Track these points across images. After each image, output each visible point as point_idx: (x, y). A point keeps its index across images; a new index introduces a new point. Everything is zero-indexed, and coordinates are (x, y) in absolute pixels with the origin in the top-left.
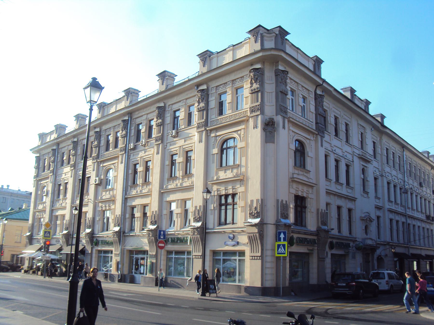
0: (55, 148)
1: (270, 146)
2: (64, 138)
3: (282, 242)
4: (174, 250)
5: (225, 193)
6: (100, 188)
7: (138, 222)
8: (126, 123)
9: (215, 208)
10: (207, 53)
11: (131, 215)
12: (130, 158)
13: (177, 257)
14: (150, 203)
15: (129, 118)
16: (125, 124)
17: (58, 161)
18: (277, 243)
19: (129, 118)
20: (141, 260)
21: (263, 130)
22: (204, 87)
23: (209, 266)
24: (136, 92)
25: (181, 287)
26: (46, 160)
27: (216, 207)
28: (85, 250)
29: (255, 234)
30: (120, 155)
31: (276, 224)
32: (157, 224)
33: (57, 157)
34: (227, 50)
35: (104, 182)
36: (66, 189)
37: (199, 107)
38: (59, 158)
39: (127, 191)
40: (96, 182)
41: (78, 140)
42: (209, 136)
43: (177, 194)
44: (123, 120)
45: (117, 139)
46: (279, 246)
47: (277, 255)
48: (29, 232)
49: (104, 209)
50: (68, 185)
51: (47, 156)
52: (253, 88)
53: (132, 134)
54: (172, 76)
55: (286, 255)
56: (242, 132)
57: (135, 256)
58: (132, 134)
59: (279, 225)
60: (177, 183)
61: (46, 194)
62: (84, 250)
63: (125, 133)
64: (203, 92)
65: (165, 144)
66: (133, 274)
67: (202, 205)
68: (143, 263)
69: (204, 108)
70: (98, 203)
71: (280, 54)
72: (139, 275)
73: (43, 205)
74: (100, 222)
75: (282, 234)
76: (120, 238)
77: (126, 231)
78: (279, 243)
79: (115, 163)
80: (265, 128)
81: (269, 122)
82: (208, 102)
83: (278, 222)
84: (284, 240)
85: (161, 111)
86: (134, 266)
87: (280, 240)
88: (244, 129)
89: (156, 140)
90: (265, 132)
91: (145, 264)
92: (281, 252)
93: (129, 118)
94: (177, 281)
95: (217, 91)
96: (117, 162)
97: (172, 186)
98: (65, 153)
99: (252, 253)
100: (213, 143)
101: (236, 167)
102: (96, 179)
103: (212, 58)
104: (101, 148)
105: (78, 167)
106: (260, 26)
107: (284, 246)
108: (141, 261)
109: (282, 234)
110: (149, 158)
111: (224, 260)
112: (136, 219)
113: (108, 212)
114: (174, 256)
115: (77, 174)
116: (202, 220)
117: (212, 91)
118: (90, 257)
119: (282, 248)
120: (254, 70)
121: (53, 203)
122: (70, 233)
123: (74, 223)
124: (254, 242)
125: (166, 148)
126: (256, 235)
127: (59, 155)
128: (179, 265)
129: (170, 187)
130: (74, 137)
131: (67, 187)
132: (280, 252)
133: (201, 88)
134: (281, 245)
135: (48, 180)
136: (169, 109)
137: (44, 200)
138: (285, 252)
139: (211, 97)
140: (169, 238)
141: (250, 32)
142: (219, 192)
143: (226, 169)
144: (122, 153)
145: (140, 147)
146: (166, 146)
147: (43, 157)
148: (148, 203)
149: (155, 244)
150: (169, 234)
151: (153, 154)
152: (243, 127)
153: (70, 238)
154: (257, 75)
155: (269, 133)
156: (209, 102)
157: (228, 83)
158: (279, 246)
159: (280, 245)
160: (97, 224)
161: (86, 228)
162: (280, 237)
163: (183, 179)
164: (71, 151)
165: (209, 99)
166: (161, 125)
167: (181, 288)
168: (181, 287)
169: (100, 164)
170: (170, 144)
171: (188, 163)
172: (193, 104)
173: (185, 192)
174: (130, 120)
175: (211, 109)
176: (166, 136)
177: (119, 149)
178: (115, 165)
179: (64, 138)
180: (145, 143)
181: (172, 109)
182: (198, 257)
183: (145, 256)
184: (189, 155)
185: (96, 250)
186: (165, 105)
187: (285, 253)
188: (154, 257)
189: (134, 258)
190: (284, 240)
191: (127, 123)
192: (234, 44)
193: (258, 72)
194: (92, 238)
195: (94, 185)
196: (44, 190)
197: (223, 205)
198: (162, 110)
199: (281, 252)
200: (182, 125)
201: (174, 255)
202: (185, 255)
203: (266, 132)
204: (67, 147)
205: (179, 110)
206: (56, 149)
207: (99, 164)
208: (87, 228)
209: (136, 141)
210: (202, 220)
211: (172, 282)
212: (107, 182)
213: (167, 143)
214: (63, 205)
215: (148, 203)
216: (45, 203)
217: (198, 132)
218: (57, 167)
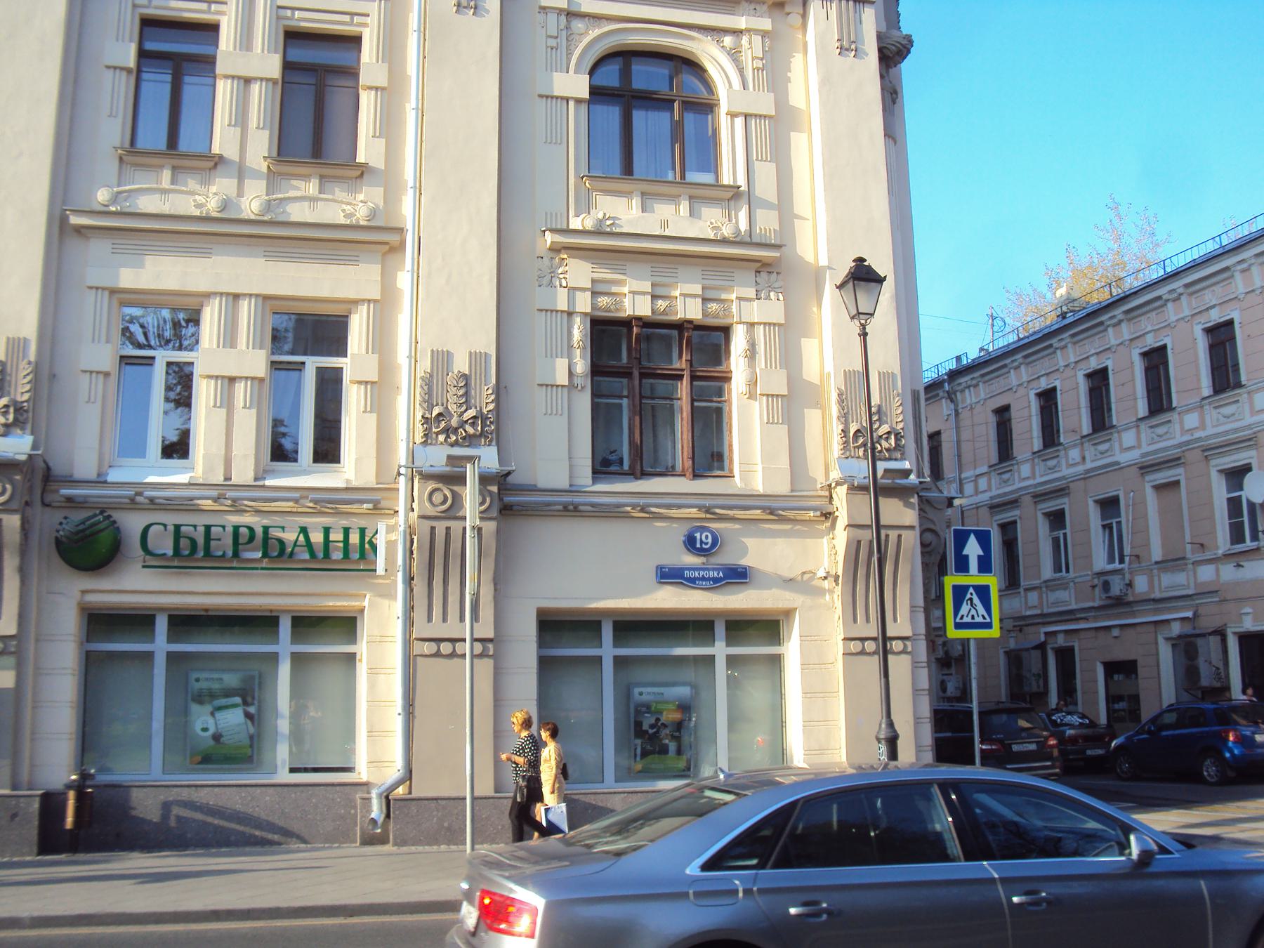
3: (974, 578)
4: (162, 609)
5: (594, 307)
25: (276, 837)
43: (216, 259)
46: (960, 592)
47: (952, 633)
67: (897, 370)
75: (972, 538)
78: (961, 580)
88: (764, 34)
92: (973, 617)
94: (235, 801)
99: (855, 621)
101: (722, 200)
107: (983, 592)
109: (972, 538)
119: (976, 600)
126: (448, 529)
128: (201, 702)
132: (967, 620)
134: (971, 590)
142: (603, 301)
143: (649, 194)
158: (960, 592)
159: (966, 588)
162: (965, 552)
163: (273, 178)
167: (279, 844)
168: (276, 837)
173: (291, 257)
187: (988, 626)
188: (874, 653)
190: (985, 566)
199: (973, 617)
202: (152, 639)
211: (176, 811)
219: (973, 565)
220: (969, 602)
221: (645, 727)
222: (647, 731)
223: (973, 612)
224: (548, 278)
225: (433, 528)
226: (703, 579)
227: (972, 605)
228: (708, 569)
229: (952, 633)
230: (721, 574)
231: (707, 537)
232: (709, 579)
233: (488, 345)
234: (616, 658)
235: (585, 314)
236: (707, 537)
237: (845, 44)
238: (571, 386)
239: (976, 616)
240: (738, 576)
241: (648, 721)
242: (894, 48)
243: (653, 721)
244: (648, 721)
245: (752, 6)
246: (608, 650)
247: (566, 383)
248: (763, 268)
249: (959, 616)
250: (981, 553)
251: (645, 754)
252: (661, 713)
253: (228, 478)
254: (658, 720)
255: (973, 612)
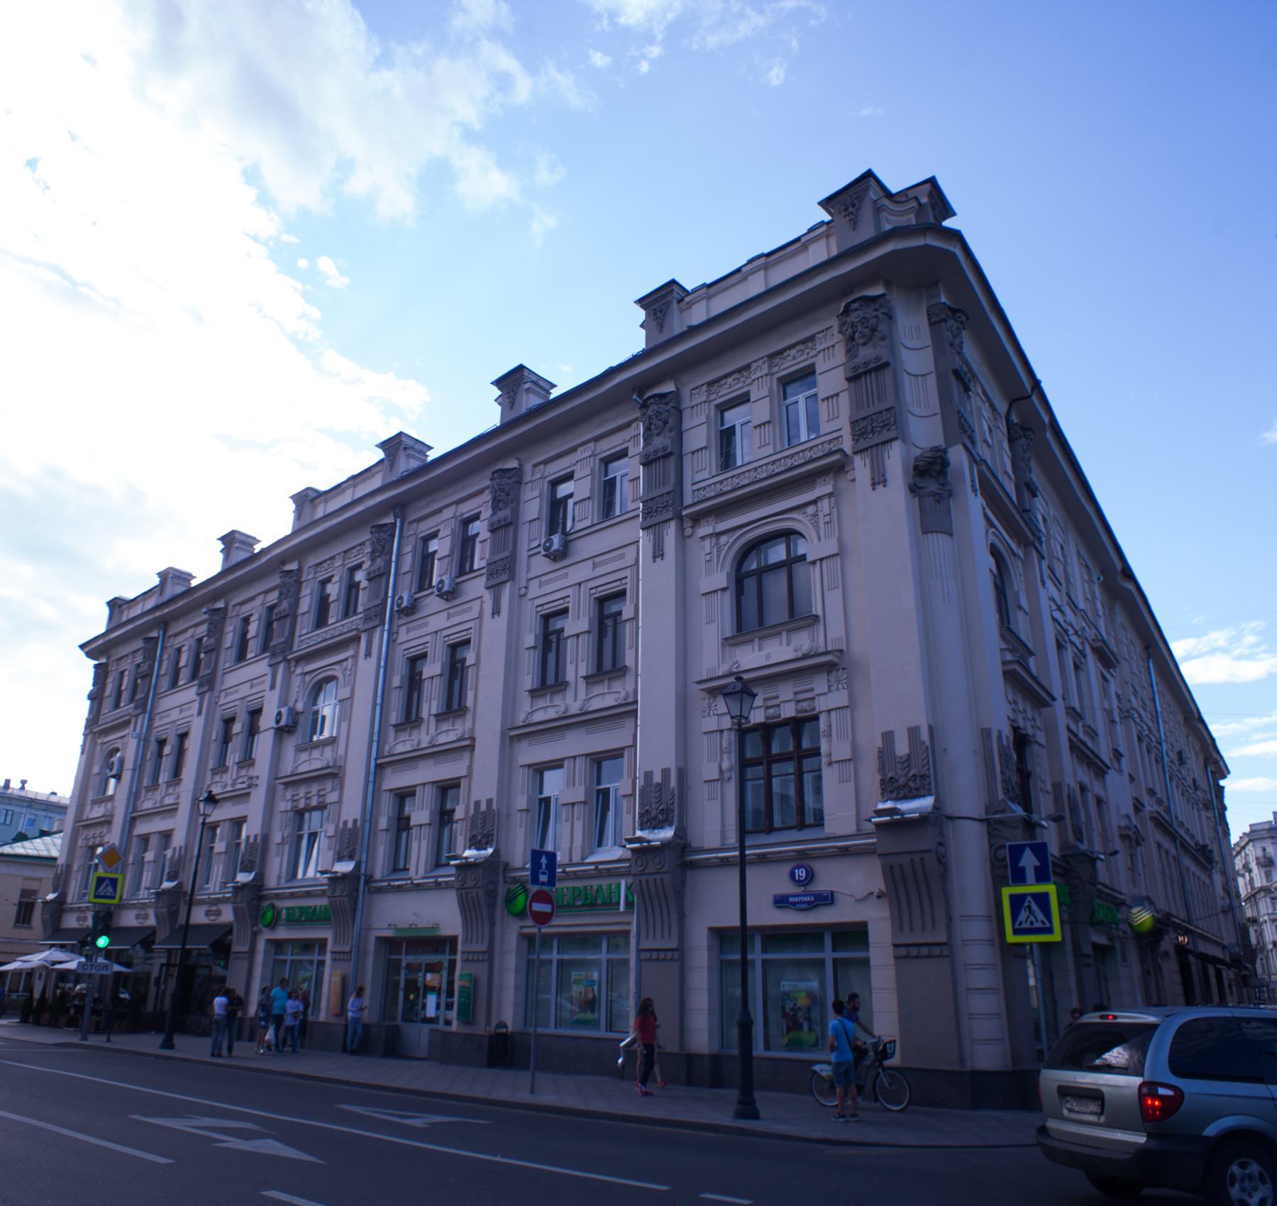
0: (156, 635)
1: (938, 542)
2: (186, 601)
6: (290, 743)
7: (576, 822)
8: (388, 533)
9: (726, 775)
10: (673, 290)
11: (396, 821)
12: (395, 640)
13: (566, 957)
14: (469, 775)
15: (398, 520)
16: (385, 536)
17: (163, 672)
18: (1007, 892)
19: (396, 521)
20: (427, 971)
21: (908, 490)
22: (293, 566)
23: (709, 989)
24: (418, 447)
26: (126, 673)
27: (287, 837)
28: (231, 940)
29: (917, 858)
30: (365, 631)
31: (987, 819)
32: (494, 844)
33: (161, 662)
34: (803, 240)
35: (304, 722)
36: (180, 753)
37: (651, 449)
38: (165, 664)
39: (384, 744)
40: (278, 721)
41: (227, 604)
42: (689, 537)
44: (145, 639)
45: (352, 587)
46: (1017, 901)
47: (1011, 938)
48: (54, 892)
49: (302, 805)
50: (187, 741)
51: (129, 661)
52: (856, 362)
53: (406, 566)
54: (249, 541)
55: (1056, 937)
56: (825, 505)
57: (406, 959)
58: (406, 566)
59: (1001, 822)
60: (423, 737)
61: (118, 770)
62: (227, 942)
63: (382, 564)
64: (664, 401)
65: (523, 584)
66: (399, 1021)
68: (435, 984)
69: (382, 571)
70: (282, 787)
71: (951, 249)
72: (419, 1025)
73: (105, 807)
74: (287, 848)
75: (1028, 852)
76: (357, 897)
77: (378, 875)
79: (346, 660)
80: (915, 485)
81: (930, 463)
82: (681, 433)
83: (996, 812)
84: (1042, 877)
85: (509, 481)
86: (401, 994)
87: (1019, 877)
88: (830, 495)
89: (366, 619)
90: (917, 499)
91: (444, 986)
92: (1032, 923)
93: (398, 520)
95: (135, 660)
96: (353, 656)
97: (403, 745)
98: (252, 619)
100: (708, 558)
102: (279, 714)
103: (688, 303)
104: (299, 619)
105: (222, 684)
106: (673, 282)
107: (1042, 899)
108: (429, 976)
109: (1028, 852)
110: (465, 633)
111: (561, 963)
112: (414, 832)
113: (316, 815)
114: (555, 956)
115: (220, 703)
116: (676, 819)
117: (112, 667)
118: (244, 964)
119: (1034, 907)
120: (863, 303)
121: (134, 797)
122: (184, 889)
123: (198, 856)
124: (473, 913)
125: (525, 595)
127: (165, 657)
129: (400, 748)
130: (216, 596)
131: (186, 747)
132: (1025, 925)
133: (288, 567)
134: (1029, 898)
135: (126, 732)
136: (309, 578)
137: (110, 792)
138: (1048, 925)
139: (692, 418)
140: (282, 908)
141: (827, 203)
144: (370, 625)
145: (432, 603)
146: (526, 588)
147: (118, 665)
148: (624, 746)
149: (485, 913)
150: (393, 886)
151: (480, 617)
152: (828, 489)
153: (182, 902)
154: (667, 411)
155: (931, 499)
156: (684, 434)
157: (754, 366)
158: (1017, 901)
160: (277, 856)
161: (239, 868)
162: (1021, 864)
164: (205, 639)
165: (683, 425)
166: (504, 528)
169: (295, 666)
170: (540, 582)
171: (457, 678)
172: (570, 472)
174: (161, 638)
175: (693, 453)
176: (690, 493)
177: (361, 615)
178: (347, 666)
179: (186, 601)
180: (450, 585)
181: (419, 531)
182: (476, 958)
183: (445, 958)
184: (458, 657)
185: (269, 941)
186: (521, 465)
187: (1050, 930)
189: (404, 964)
191: (389, 535)
192: (708, 281)
193: (876, 310)
194: (255, 902)
195: (272, 732)
196: (112, 760)
197: (755, 762)
198: (513, 479)
199: (1032, 923)
200: (580, 516)
201: (555, 951)
202: (601, 953)
203: (920, 498)
204: (262, 596)
205: (434, 535)
206: (158, 638)
207: (293, 669)
208: (241, 871)
209: (417, 588)
210: (676, 819)
212: (315, 722)
213: (529, 580)
214: (168, 800)
215: (460, 778)
216: (112, 798)
217: (270, 666)
218: (158, 692)
219: (1030, 874)
220: (1027, 910)
221: (787, 1010)
222: (788, 1014)
223: (1031, 918)
224: (707, 711)
225: (912, 860)
226: (801, 902)
227: (1030, 911)
228: (804, 896)
229: (1011, 938)
230: (812, 898)
231: (802, 872)
232: (804, 903)
233: (671, 763)
234: (835, 960)
235: (730, 729)
236: (802, 872)
237: (876, 480)
238: (721, 779)
239: (1035, 922)
240: (826, 899)
241: (789, 1005)
242: (922, 463)
243: (792, 1006)
244: (789, 1005)
245: (822, 479)
246: (828, 954)
247: (833, 759)
248: (829, 668)
249: (1018, 922)
250: (1038, 864)
251: (789, 1030)
252: (797, 999)
253: (571, 860)
254: (795, 1005)
255: (1031, 918)
